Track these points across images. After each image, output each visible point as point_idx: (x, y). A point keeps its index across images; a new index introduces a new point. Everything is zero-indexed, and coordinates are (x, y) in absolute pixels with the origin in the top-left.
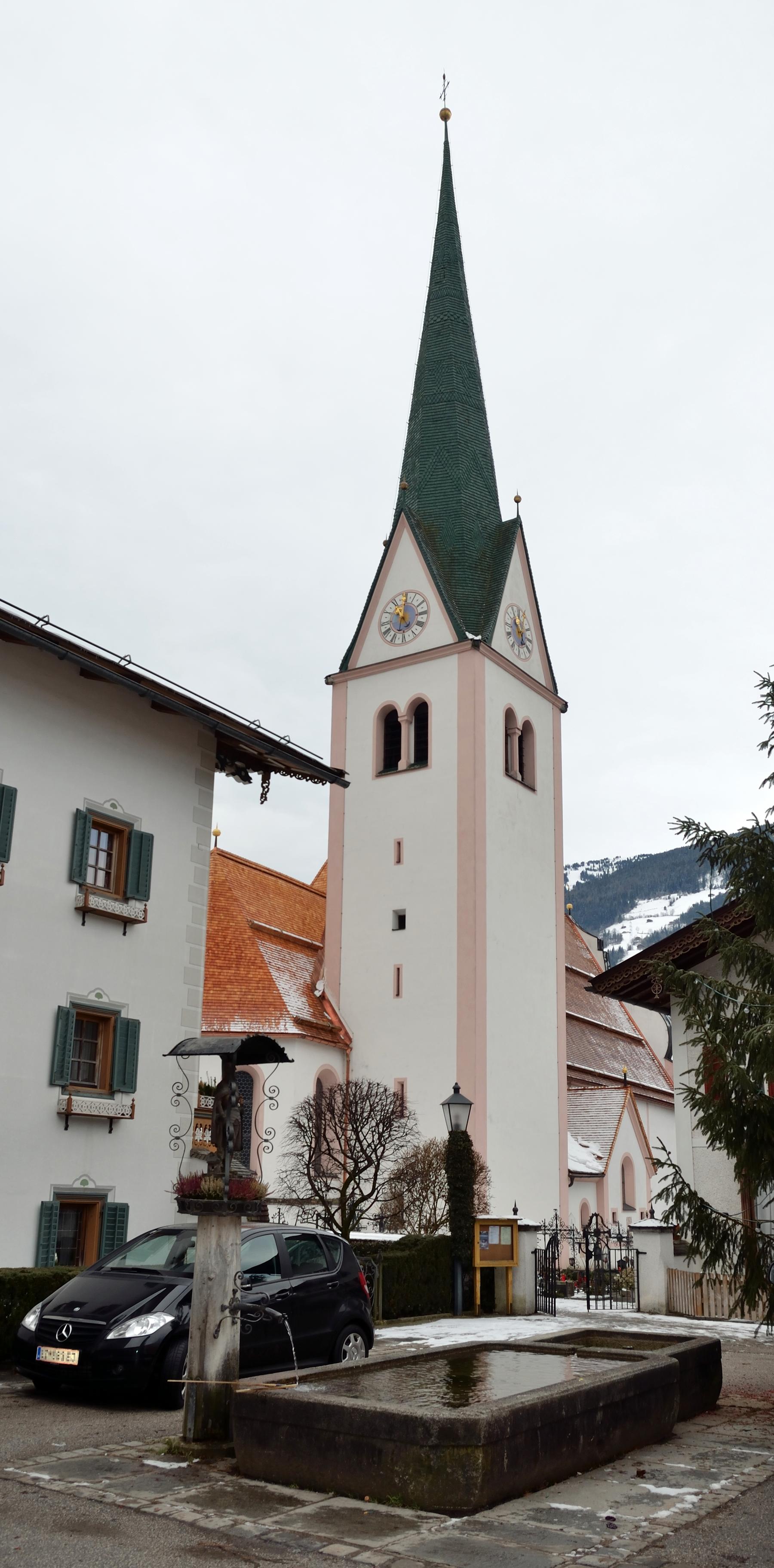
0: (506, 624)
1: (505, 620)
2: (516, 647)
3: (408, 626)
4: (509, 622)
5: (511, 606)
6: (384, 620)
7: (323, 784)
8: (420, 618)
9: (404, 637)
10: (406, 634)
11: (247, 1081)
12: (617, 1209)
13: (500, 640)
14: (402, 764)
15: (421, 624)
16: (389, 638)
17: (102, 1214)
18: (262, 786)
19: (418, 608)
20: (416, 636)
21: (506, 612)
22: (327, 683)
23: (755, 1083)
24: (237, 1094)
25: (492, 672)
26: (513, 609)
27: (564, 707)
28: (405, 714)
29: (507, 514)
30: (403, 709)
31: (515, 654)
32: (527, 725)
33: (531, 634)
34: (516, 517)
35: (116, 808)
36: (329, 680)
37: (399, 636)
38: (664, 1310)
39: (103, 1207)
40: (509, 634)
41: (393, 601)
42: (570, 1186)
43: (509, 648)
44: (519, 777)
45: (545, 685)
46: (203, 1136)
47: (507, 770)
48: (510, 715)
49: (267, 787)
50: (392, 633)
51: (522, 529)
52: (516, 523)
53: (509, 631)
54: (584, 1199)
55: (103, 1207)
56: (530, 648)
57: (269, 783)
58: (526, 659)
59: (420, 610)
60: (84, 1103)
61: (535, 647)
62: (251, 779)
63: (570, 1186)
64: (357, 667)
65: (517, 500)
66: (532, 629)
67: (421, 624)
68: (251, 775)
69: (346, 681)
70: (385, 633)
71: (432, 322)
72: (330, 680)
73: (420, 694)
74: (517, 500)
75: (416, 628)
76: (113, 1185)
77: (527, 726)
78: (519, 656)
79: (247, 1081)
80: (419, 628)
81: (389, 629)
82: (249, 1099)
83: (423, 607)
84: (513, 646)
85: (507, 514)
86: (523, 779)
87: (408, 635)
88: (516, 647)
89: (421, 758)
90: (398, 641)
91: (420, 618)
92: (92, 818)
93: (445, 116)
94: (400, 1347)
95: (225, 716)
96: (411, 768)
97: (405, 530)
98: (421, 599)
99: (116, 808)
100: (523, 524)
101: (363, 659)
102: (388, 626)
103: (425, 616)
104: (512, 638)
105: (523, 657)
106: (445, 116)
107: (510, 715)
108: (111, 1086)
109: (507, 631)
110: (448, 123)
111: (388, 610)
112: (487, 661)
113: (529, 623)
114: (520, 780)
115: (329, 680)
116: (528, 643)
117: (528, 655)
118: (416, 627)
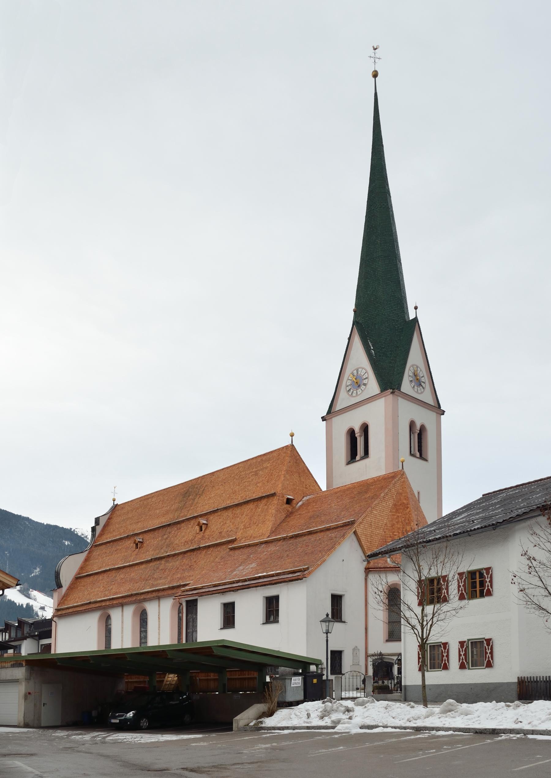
0: (410, 376)
2: (416, 387)
3: (359, 386)
4: (411, 375)
5: (413, 366)
6: (348, 384)
9: (357, 392)
10: (358, 391)
13: (406, 386)
14: (358, 458)
15: (365, 385)
16: (350, 393)
19: (363, 376)
21: (409, 370)
23: (63, 541)
25: (402, 402)
27: (443, 413)
28: (358, 432)
29: (412, 316)
30: (357, 430)
31: (415, 391)
33: (426, 379)
34: (415, 317)
36: (323, 419)
37: (355, 392)
38: (515, 694)
40: (411, 381)
43: (412, 389)
44: (418, 454)
45: (433, 405)
48: (412, 425)
50: (352, 390)
52: (416, 320)
53: (412, 379)
56: (424, 386)
58: (422, 393)
59: (364, 377)
61: (427, 386)
64: (336, 411)
65: (416, 308)
66: (426, 376)
67: (365, 385)
69: (332, 418)
70: (349, 391)
72: (324, 419)
73: (352, 426)
74: (416, 308)
75: (363, 387)
77: (423, 429)
78: (417, 392)
80: (364, 387)
81: (350, 389)
83: (366, 375)
84: (414, 387)
85: (412, 316)
87: (359, 391)
88: (416, 387)
90: (354, 395)
93: (375, 75)
96: (362, 458)
97: (356, 335)
98: (365, 371)
100: (419, 320)
101: (338, 406)
102: (350, 387)
103: (367, 380)
104: (413, 383)
105: (419, 392)
106: (375, 75)
112: (400, 399)
113: (422, 372)
115: (323, 419)
116: (422, 384)
117: (422, 390)
118: (363, 386)
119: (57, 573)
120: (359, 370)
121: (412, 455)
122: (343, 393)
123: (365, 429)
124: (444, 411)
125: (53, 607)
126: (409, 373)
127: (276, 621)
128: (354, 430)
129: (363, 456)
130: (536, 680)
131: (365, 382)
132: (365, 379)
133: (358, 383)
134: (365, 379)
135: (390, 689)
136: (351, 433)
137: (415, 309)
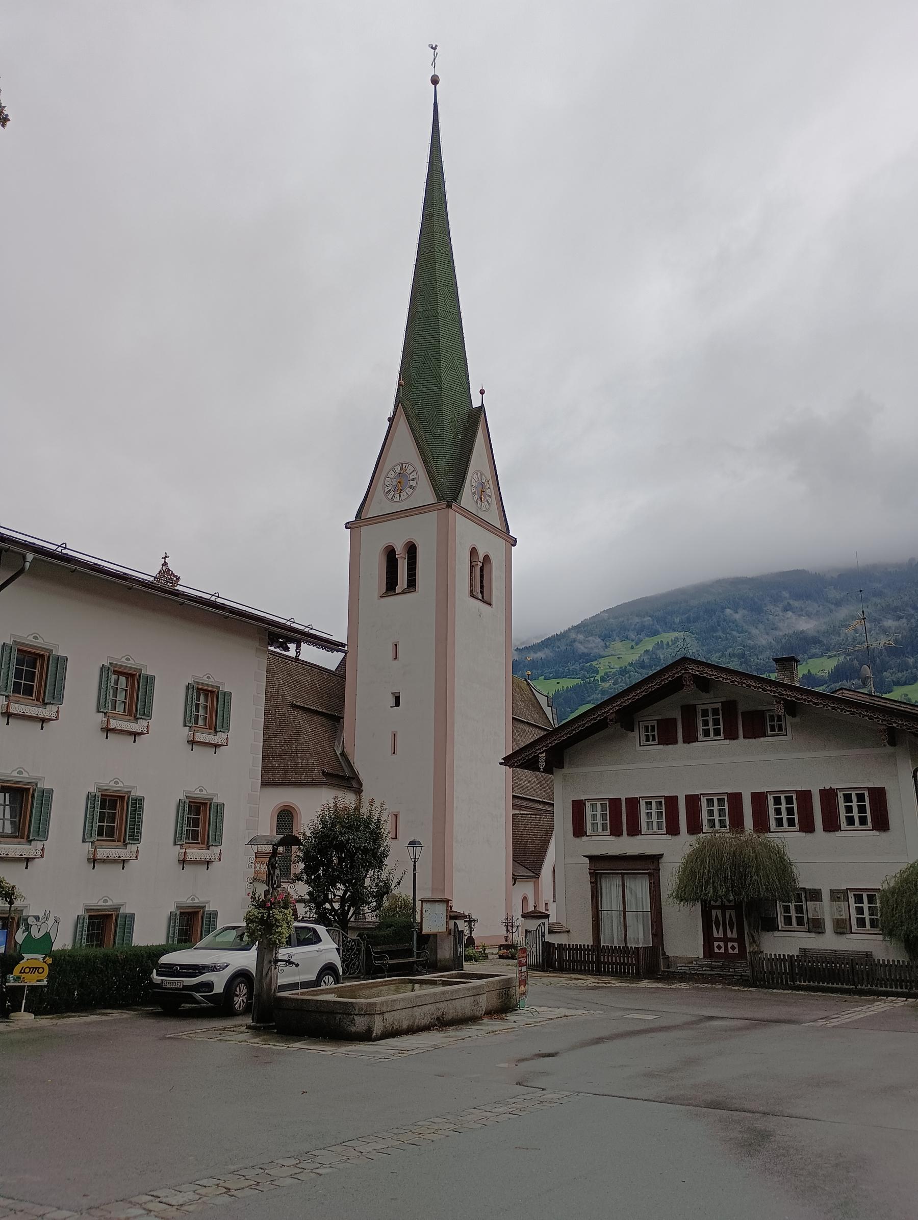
1: (471, 484)
7: (332, 652)
8: (411, 483)
9: (400, 496)
11: (289, 816)
12: (549, 901)
13: (467, 498)
14: (398, 589)
15: (411, 487)
17: (202, 917)
18: (296, 652)
20: (409, 496)
22: (347, 528)
24: (278, 862)
26: (477, 474)
27: (514, 542)
29: (476, 404)
32: (487, 558)
35: (210, 679)
39: (203, 913)
41: (393, 469)
42: (514, 885)
46: (260, 868)
47: (471, 591)
48: (474, 551)
49: (299, 652)
51: (485, 414)
52: (482, 408)
54: (525, 894)
55: (203, 913)
57: (300, 650)
58: (487, 510)
60: (194, 853)
62: (289, 648)
63: (514, 885)
65: (482, 392)
66: (492, 487)
67: (411, 487)
68: (289, 645)
70: (387, 492)
71: (423, 253)
74: (482, 392)
76: (208, 900)
79: (289, 816)
82: (290, 829)
83: (413, 476)
85: (476, 404)
86: (483, 597)
89: (412, 583)
90: (396, 499)
91: (411, 483)
92: (196, 686)
93: (435, 81)
94: (546, 947)
95: (273, 621)
96: (404, 592)
99: (210, 679)
101: (371, 512)
102: (390, 488)
106: (435, 81)
107: (474, 551)
108: (208, 842)
109: (473, 491)
110: (437, 86)
111: (389, 476)
114: (481, 599)
119: (420, 972)
120: (404, 465)
121: (472, 595)
122: (379, 492)
123: (412, 550)
124: (515, 540)
125: (3, 794)
126: (471, 482)
127: (399, 706)
128: (394, 549)
129: (406, 589)
130: (904, 978)
131: (413, 483)
132: (412, 480)
133: (401, 483)
134: (412, 480)
135: (7, 795)
136: (391, 555)
137: (481, 393)
